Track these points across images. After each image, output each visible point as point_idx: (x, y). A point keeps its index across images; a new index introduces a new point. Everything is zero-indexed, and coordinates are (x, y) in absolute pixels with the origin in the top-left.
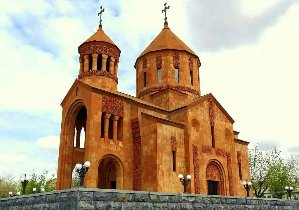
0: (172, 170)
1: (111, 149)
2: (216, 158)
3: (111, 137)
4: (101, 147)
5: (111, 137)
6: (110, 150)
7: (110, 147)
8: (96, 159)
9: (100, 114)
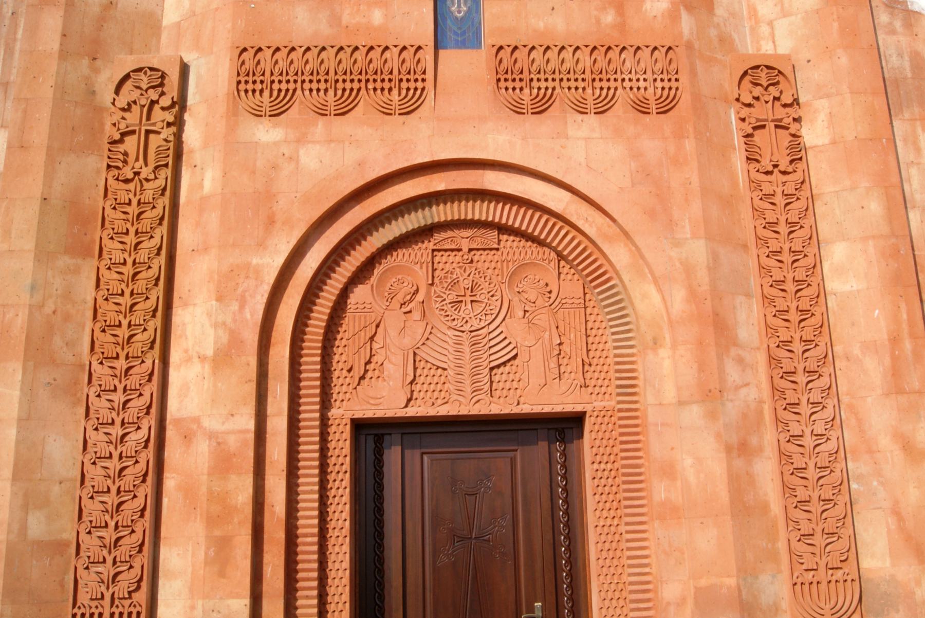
0: (809, 83)
2: (499, 139)
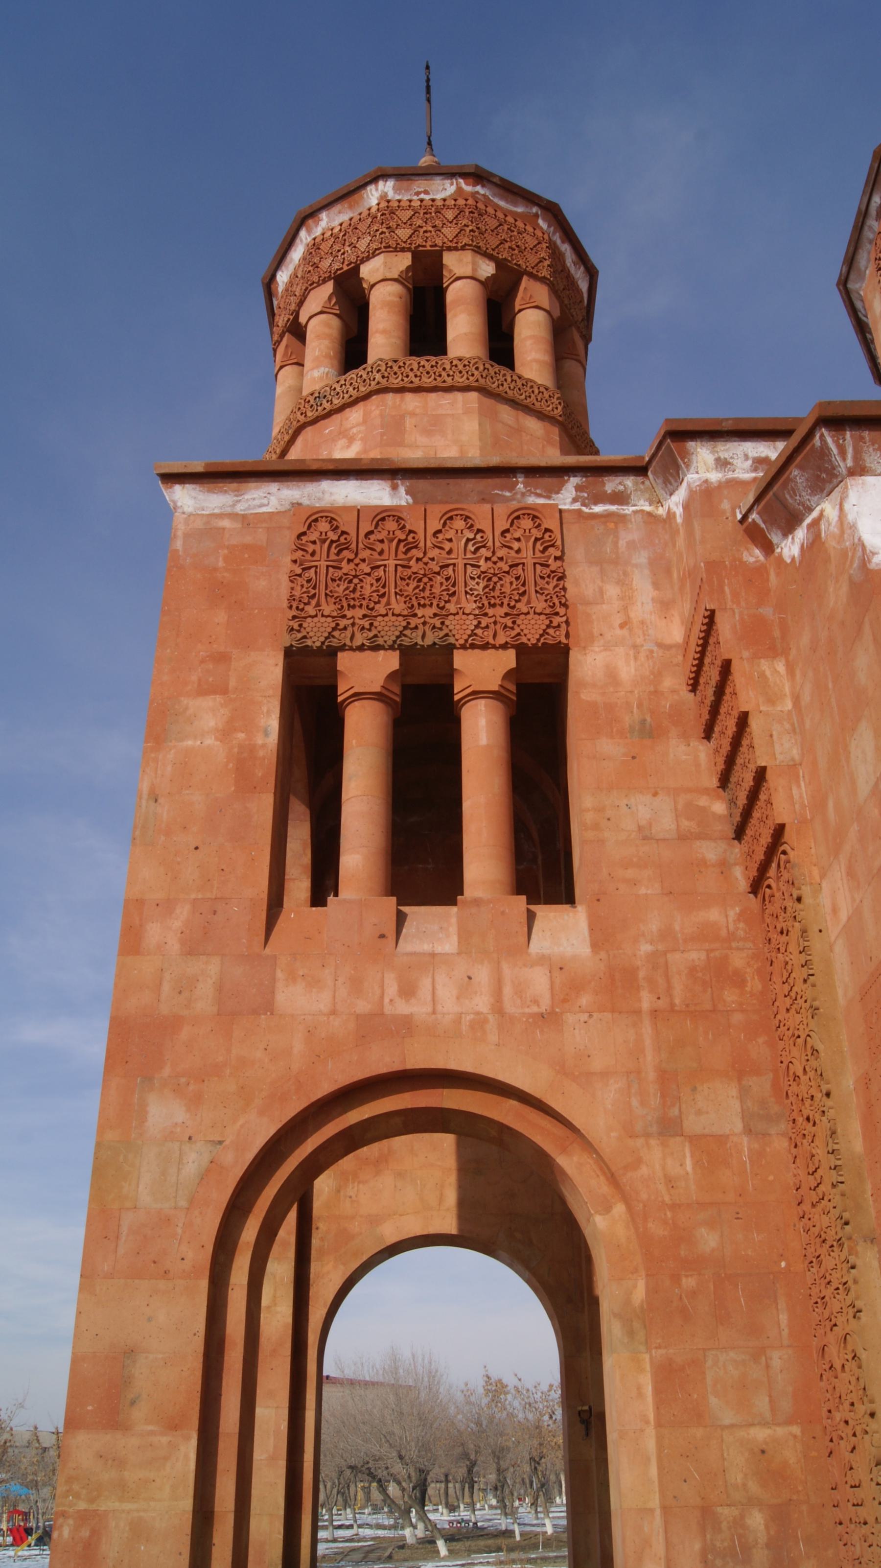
1: (417, 1009)
3: (423, 866)
4: (268, 1007)
5: (423, 866)
6: (406, 1027)
7: (408, 991)
8: (194, 1161)
9: (270, 671)
